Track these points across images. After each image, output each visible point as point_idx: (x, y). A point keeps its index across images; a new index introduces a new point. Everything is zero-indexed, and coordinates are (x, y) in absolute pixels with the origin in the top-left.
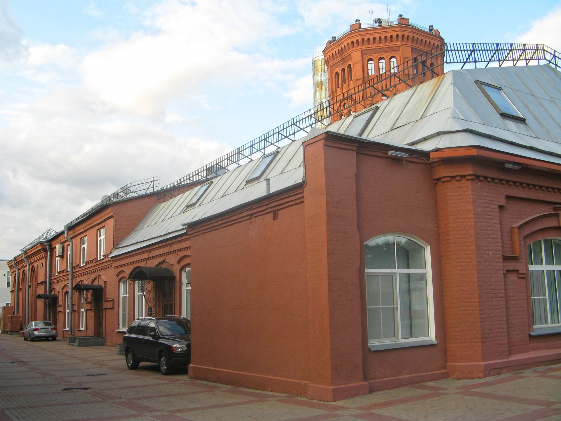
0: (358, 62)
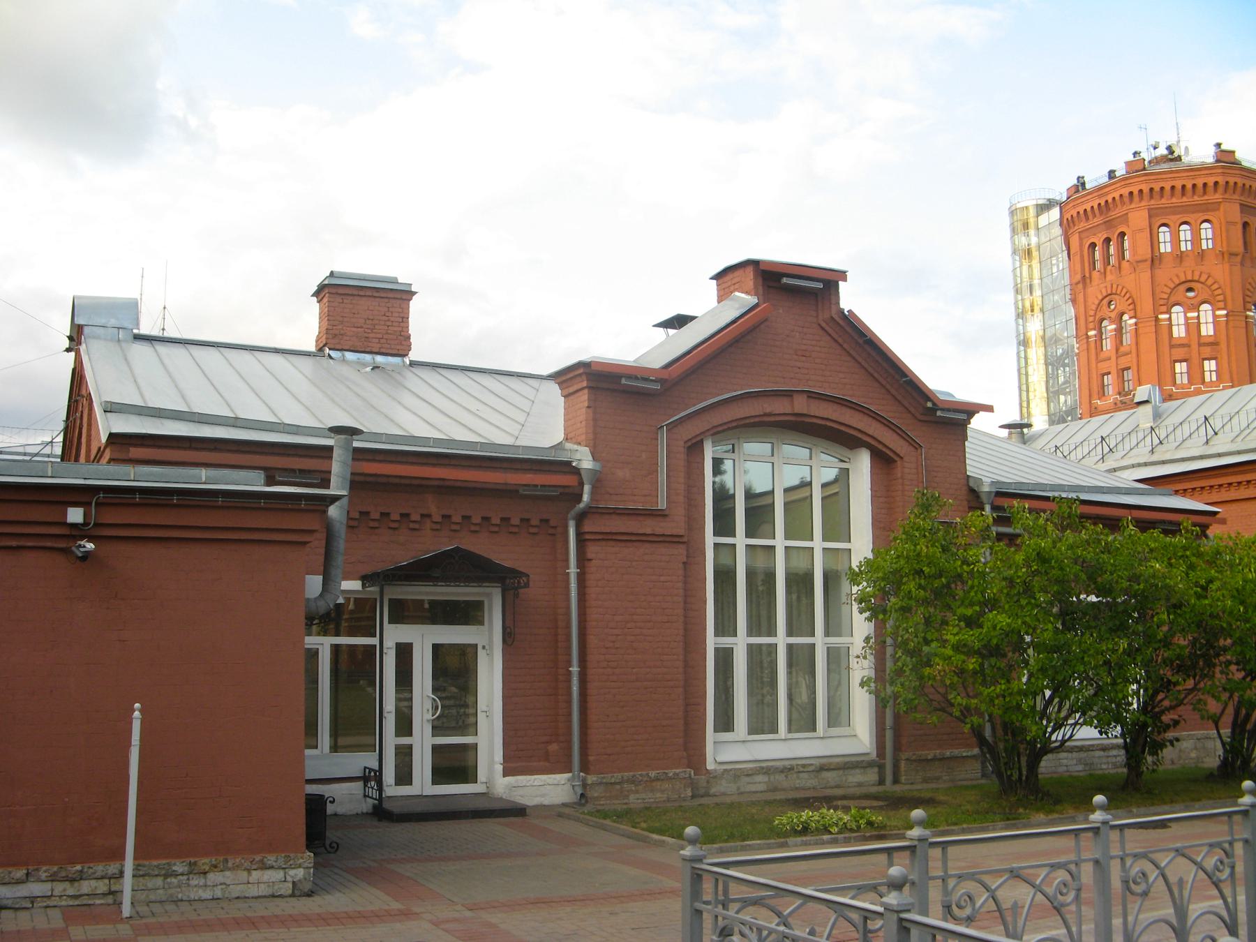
0: (1141, 230)
